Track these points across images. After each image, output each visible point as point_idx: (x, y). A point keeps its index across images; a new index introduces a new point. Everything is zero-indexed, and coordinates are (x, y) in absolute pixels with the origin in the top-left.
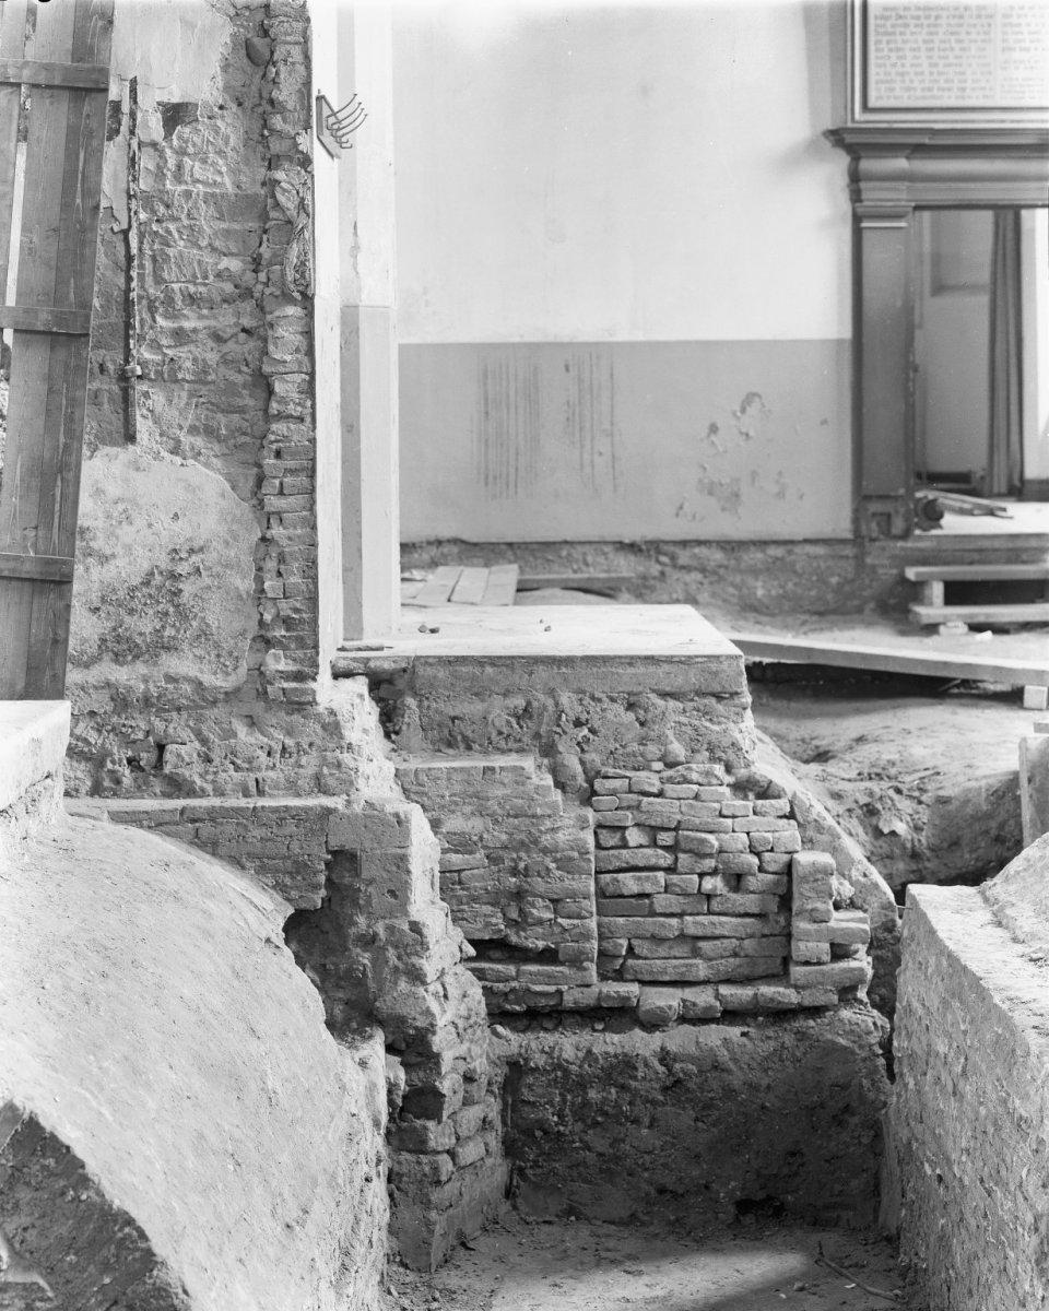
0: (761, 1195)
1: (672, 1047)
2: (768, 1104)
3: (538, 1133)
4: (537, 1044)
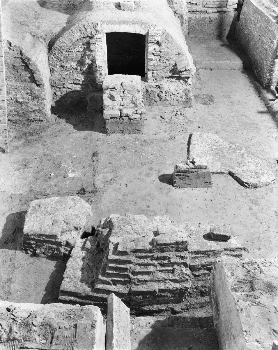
0: (143, 311)
1: (211, 16)
2: (141, 333)
3: (193, 27)
4: (193, 16)
